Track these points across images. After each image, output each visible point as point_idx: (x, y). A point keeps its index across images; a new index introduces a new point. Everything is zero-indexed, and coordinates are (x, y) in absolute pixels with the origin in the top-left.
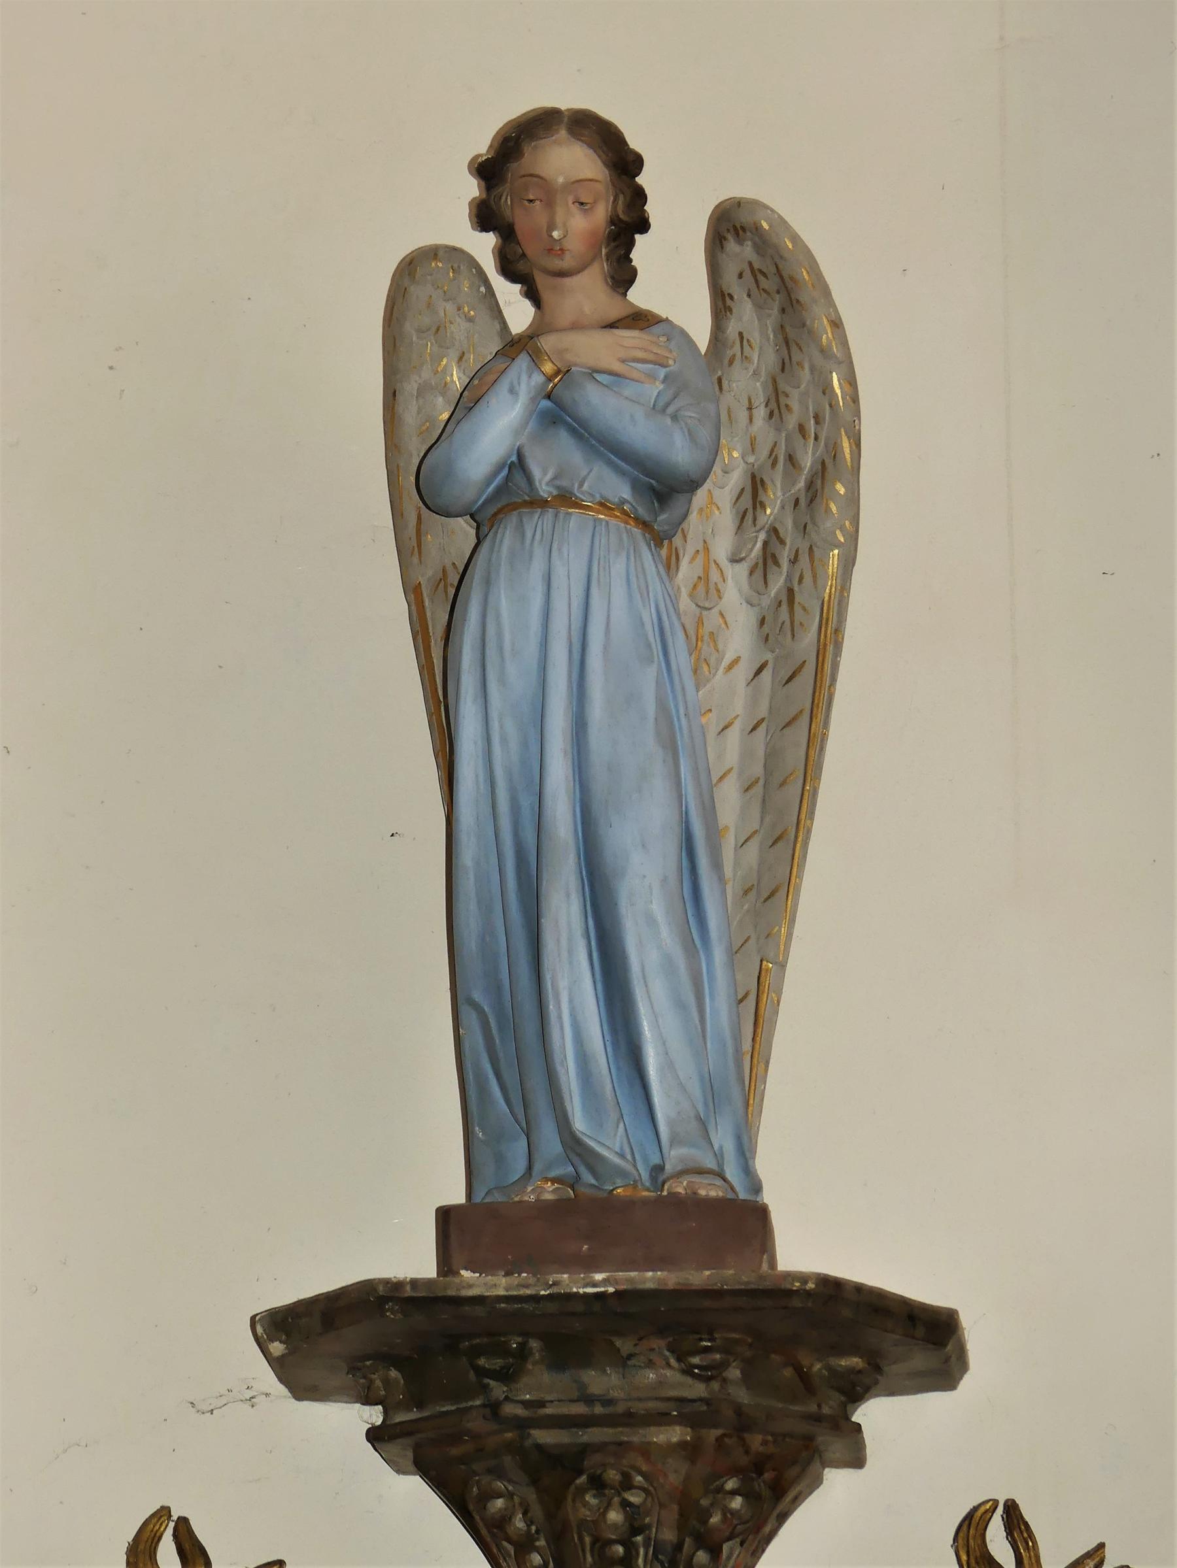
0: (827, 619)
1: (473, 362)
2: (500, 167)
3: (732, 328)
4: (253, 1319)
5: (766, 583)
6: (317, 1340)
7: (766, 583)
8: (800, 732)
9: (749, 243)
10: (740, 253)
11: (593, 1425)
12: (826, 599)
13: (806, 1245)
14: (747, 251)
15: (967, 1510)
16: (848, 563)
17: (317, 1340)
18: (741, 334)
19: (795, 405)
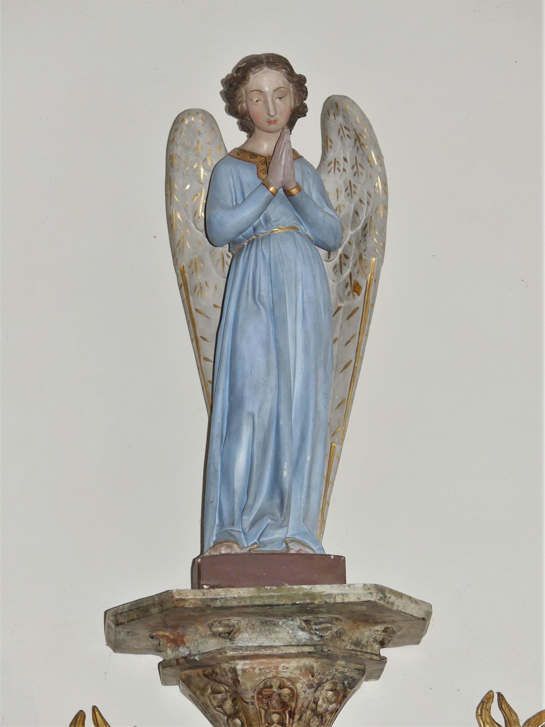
0: (367, 300)
1: (211, 163)
2: (234, 87)
3: (331, 155)
4: (106, 613)
5: (341, 272)
6: (138, 623)
7: (341, 272)
8: (353, 345)
9: (341, 116)
10: (336, 122)
11: (294, 654)
12: (369, 281)
13: (327, 553)
14: (340, 119)
15: (174, 119)
16: (380, 262)
17: (138, 623)
18: (335, 159)
19: (358, 191)
